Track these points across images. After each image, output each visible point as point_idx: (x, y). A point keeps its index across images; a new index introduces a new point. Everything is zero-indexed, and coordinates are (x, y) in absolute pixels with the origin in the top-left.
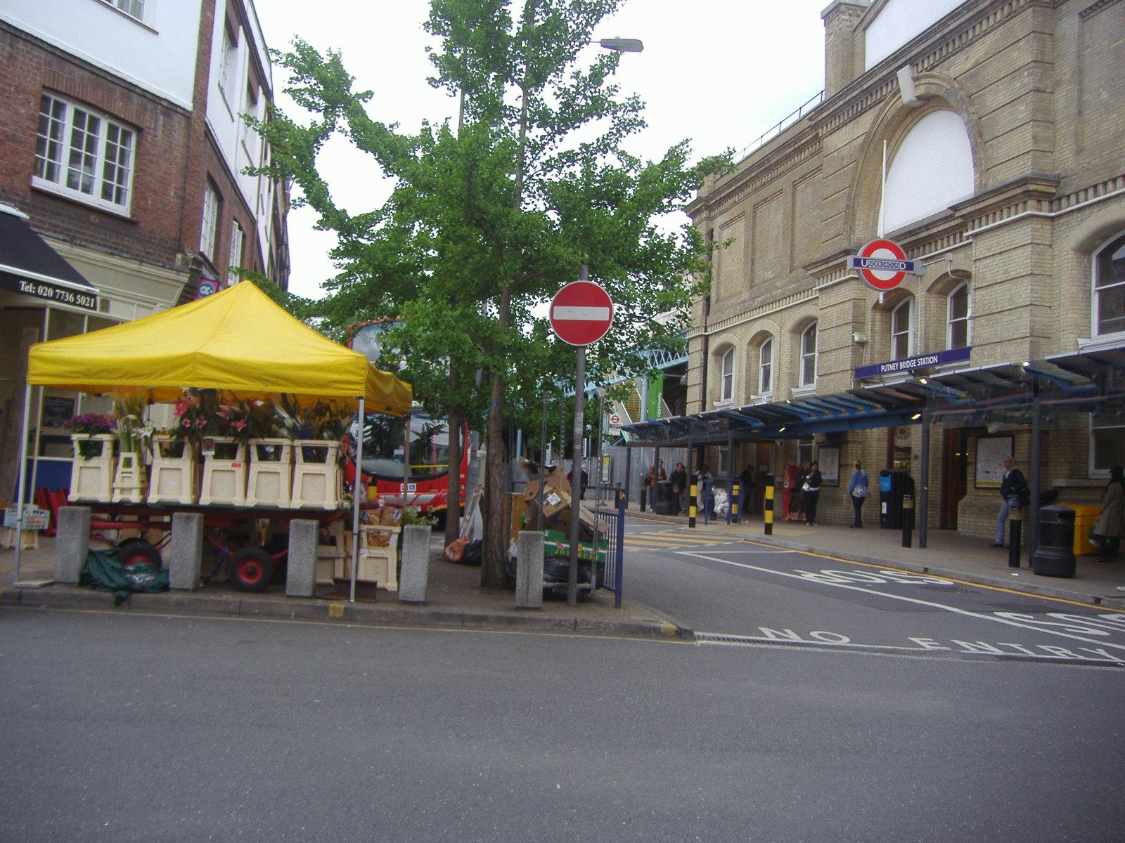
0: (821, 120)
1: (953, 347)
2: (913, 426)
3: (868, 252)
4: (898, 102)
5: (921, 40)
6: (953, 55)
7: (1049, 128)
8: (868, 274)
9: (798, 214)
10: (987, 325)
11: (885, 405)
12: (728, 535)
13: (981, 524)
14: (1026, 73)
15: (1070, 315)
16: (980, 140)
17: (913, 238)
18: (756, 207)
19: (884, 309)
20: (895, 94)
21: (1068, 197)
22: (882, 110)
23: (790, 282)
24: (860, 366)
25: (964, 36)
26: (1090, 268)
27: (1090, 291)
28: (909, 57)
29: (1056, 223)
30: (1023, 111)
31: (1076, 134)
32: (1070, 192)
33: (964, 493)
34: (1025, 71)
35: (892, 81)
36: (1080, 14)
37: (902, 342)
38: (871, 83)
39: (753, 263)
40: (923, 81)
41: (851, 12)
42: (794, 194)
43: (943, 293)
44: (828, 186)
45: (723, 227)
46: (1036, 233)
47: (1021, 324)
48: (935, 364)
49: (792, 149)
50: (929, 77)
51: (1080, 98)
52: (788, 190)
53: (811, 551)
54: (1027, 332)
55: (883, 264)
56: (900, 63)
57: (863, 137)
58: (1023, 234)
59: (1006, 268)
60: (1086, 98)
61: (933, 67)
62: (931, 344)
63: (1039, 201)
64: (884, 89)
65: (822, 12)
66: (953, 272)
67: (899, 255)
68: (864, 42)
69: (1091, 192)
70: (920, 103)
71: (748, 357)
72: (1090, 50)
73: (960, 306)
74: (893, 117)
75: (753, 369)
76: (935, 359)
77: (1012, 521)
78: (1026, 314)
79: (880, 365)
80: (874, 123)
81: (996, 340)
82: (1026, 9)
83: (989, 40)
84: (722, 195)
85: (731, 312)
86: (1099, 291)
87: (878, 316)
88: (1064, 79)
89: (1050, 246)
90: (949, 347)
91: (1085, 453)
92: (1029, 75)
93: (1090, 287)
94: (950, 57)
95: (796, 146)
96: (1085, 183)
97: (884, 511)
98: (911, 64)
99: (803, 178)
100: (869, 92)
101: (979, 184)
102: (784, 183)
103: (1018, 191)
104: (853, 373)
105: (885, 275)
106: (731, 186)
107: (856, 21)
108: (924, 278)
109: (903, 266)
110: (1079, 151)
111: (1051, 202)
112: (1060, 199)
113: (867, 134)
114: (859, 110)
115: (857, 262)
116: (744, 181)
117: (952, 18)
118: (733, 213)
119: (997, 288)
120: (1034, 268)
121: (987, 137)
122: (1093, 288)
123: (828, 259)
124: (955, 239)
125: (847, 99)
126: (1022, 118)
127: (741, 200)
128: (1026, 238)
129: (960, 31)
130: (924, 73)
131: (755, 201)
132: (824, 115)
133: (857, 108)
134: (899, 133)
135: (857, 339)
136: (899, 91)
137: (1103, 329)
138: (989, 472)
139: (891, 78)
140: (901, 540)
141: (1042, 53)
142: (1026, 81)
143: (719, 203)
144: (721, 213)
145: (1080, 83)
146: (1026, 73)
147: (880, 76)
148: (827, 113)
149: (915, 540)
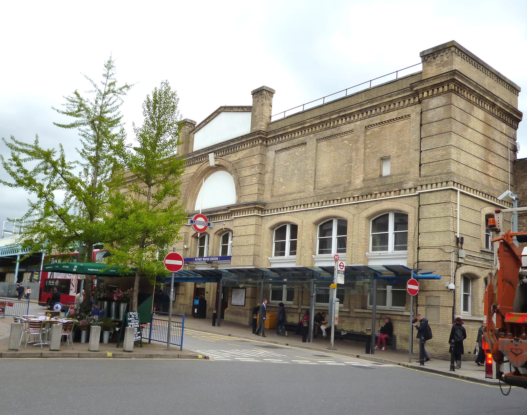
1: (222, 255)
2: (235, 290)
3: (196, 218)
4: (208, 164)
7: (263, 186)
8: (195, 226)
11: (202, 275)
14: (257, 167)
16: (239, 185)
17: (211, 214)
20: (207, 161)
21: (268, 210)
22: (201, 166)
24: (186, 258)
25: (235, 148)
26: (273, 234)
28: (214, 150)
29: (263, 218)
30: (255, 180)
31: (272, 190)
33: (227, 307)
34: (256, 166)
35: (206, 157)
36: (275, 151)
38: (198, 155)
40: (218, 160)
41: (189, 125)
47: (251, 251)
51: (273, 178)
54: (252, 254)
55: (200, 223)
56: (210, 151)
58: (253, 221)
60: (275, 179)
61: (223, 156)
62: (215, 252)
63: (259, 211)
67: (206, 220)
70: (216, 166)
72: (277, 164)
73: (225, 240)
74: (205, 169)
76: (217, 259)
78: (252, 247)
79: (195, 258)
83: (244, 152)
89: (261, 225)
90: (220, 255)
92: (259, 168)
96: (274, 207)
97: (196, 312)
98: (214, 153)
100: (197, 158)
101: (238, 201)
103: (252, 206)
105: (200, 227)
107: (191, 129)
108: (213, 229)
109: (207, 224)
110: (272, 196)
111: (262, 211)
112: (265, 211)
113: (195, 173)
114: (192, 163)
115: (192, 222)
117: (232, 142)
119: (242, 237)
121: (241, 185)
124: (226, 217)
129: (234, 147)
133: (191, 163)
134: (206, 175)
135: (185, 247)
139: (206, 156)
140: (302, 340)
141: (262, 161)
142: (256, 169)
145: (274, 174)
146: (257, 167)
147: (202, 154)
149: (216, 324)
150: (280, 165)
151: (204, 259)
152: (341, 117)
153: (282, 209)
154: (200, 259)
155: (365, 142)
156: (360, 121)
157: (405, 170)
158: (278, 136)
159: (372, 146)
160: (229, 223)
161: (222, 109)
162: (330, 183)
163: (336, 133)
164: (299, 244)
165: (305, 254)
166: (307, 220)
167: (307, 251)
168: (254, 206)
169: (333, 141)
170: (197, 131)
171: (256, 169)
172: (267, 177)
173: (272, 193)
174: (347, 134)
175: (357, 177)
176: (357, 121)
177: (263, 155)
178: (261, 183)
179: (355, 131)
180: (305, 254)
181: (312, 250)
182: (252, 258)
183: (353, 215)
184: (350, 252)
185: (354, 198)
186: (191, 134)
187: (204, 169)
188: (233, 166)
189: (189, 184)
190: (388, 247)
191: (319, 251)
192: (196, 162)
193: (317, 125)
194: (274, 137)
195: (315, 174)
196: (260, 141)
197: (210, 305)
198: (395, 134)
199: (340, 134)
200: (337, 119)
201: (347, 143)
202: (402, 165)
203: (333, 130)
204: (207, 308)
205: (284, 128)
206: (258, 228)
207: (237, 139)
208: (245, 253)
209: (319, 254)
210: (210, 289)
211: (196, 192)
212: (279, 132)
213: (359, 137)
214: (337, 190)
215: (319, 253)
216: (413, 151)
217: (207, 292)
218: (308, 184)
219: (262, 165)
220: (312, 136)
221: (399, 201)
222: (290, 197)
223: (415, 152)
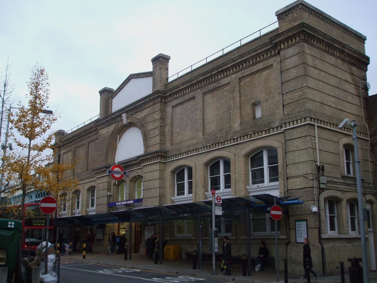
28: (125, 110)
30: (157, 132)
36: (172, 107)
40: (129, 118)
45: (63, 154)
46: (160, 167)
52: (87, 145)
53: (98, 263)
54: (158, 195)
57: (111, 132)
58: (157, 167)
61: (132, 115)
67: (122, 170)
80: (115, 128)
81: (150, 197)
83: (148, 109)
99: (92, 141)
100: (113, 119)
103: (156, 155)
106: (67, 141)
113: (113, 131)
127: (71, 146)
135: (108, 194)
136: (122, 120)
150: (177, 118)
158: (173, 94)
161: (131, 77)
162: (215, 129)
168: (157, 154)
169: (216, 93)
172: (168, 129)
175: (236, 121)
179: (231, 83)
186: (110, 99)
194: (170, 95)
196: (159, 99)
200: (217, 74)
203: (215, 84)
212: (173, 90)
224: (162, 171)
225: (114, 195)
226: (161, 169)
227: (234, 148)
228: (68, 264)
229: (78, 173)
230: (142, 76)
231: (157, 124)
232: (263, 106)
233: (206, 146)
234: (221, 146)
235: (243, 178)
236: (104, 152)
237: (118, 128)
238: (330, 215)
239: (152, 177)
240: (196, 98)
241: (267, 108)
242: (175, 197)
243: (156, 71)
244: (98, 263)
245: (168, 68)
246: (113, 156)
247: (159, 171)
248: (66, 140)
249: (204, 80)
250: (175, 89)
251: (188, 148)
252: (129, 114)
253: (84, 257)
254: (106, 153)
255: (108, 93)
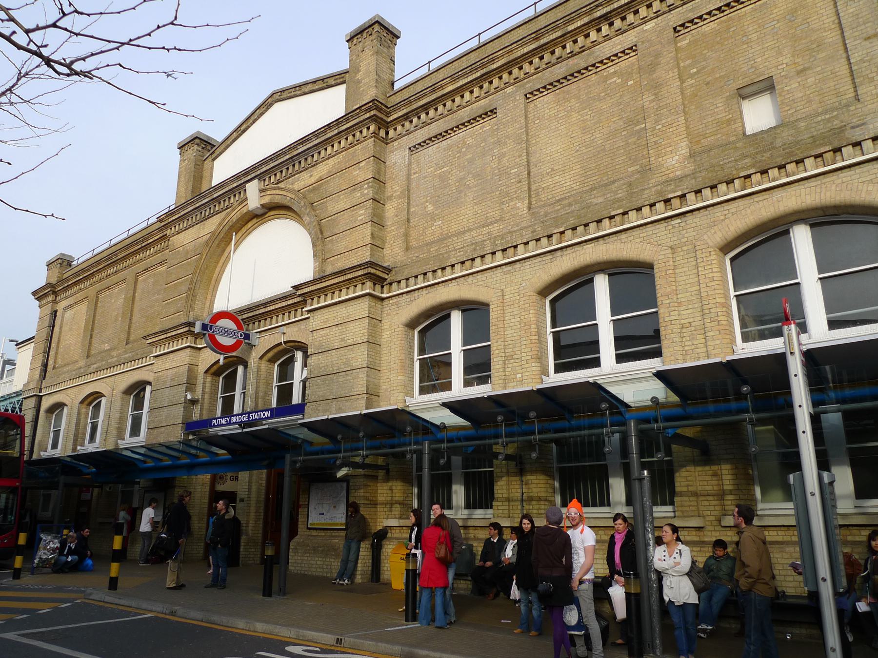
0: (171, 222)
1: (277, 406)
5: (271, 159)
6: (298, 173)
8: (212, 338)
9: (137, 298)
10: (323, 384)
12: (59, 589)
13: (314, 562)
14: (366, 186)
15: (400, 378)
18: (99, 292)
19: (215, 371)
20: (242, 202)
21: (399, 282)
23: (126, 352)
24: (190, 421)
27: (413, 359)
28: (259, 172)
29: (386, 302)
30: (363, 214)
32: (401, 278)
34: (365, 184)
36: (410, 148)
37: (228, 403)
39: (91, 337)
40: (268, 193)
41: (204, 146)
42: (136, 283)
43: (272, 361)
44: (171, 274)
45: (65, 309)
46: (372, 309)
48: (267, 418)
49: (140, 246)
50: (274, 189)
52: (131, 280)
53: (173, 613)
54: (364, 390)
56: (249, 177)
58: (362, 308)
59: (343, 336)
61: (279, 182)
62: (260, 402)
63: (375, 284)
64: (232, 199)
65: (179, 144)
66: (285, 342)
67: (239, 327)
68: (212, 169)
69: (421, 278)
71: (79, 413)
74: (238, 220)
75: (82, 424)
76: (268, 414)
77: (57, 489)
79: (211, 420)
80: (220, 224)
81: (331, 397)
82: (368, 139)
83: (332, 161)
84: (70, 283)
85: (67, 376)
86: (419, 359)
87: (209, 379)
88: (394, 195)
90: (274, 405)
91: (410, 495)
92: (369, 187)
93: (414, 356)
94: (295, 175)
95: (143, 245)
98: (259, 179)
99: (146, 270)
100: (217, 200)
101: (322, 269)
102: (128, 274)
103: (360, 273)
104: (184, 426)
106: (79, 275)
112: (391, 284)
113: (213, 233)
114: (207, 214)
116: (92, 271)
118: (77, 298)
120: (370, 337)
121: (326, 234)
122: (416, 357)
123: (168, 330)
125: (198, 205)
126: (362, 220)
127: (86, 288)
128: (363, 313)
130: (271, 186)
131: (99, 289)
132: (174, 218)
133: (205, 214)
135: (189, 397)
136: (246, 199)
137: (559, 369)
138: (323, 514)
139: (241, 188)
142: (366, 191)
143: (66, 289)
144: (67, 298)
146: (366, 186)
148: (177, 216)
150: (425, 177)
151: (234, 419)
152: (596, 24)
153: (439, 271)
154: (223, 421)
155: (678, 64)
156: (656, 20)
157: (835, 100)
158: (416, 112)
159: (704, 68)
160: (296, 329)
161: (276, 96)
162: (576, 186)
163: (583, 65)
164: (497, 352)
165: (519, 376)
166: (516, 287)
167: (526, 366)
168: (366, 271)
169: (573, 88)
170: (221, 153)
171: (366, 191)
172: (391, 210)
173: (407, 242)
174: (617, 61)
175: (669, 149)
176: (645, 20)
177: (379, 159)
178: (378, 221)
179: (640, 47)
180: (519, 376)
181: (541, 363)
182: (365, 401)
183: (672, 248)
184: (676, 348)
185: (667, 201)
186: (206, 162)
187: (234, 220)
188: (305, 197)
189: (201, 258)
190: (451, 381)
191: (555, 365)
192: (217, 209)
193: (524, 60)
194: (407, 117)
195: (529, 174)
196: (373, 128)
197: (250, 532)
198: (775, 22)
199: (593, 65)
200: (583, 31)
201: (617, 82)
202: (822, 89)
203: (571, 62)
204: (243, 538)
205: (434, 88)
206: (375, 326)
207: (315, 134)
208: (342, 392)
209: (555, 373)
210: (249, 490)
211: (215, 276)
213: (658, 55)
214: (604, 195)
215: (621, 358)
216: (858, 42)
217: (242, 500)
218: (511, 200)
219: (378, 181)
220: (509, 90)
221: (839, 181)
222: (458, 243)
223: (864, 43)
224: (375, 321)
225: (203, 399)
226: (373, 316)
227: (670, 227)
228: (46, 620)
229: (101, 352)
230: (310, 87)
231: (363, 195)
232: (785, 89)
233: (546, 234)
234: (610, 228)
235: (721, 318)
236: (184, 288)
237: (230, 223)
238: (432, 473)
239: (343, 340)
240: (498, 111)
241: (808, 92)
242: (413, 397)
243: (360, 62)
244: (173, 613)
245: (394, 57)
246: (209, 297)
247: (366, 321)
248: (77, 274)
249: (534, 55)
250: (580, 17)
251: (475, 250)
252: (267, 183)
253: (113, 584)
254: (189, 289)
255: (203, 148)
